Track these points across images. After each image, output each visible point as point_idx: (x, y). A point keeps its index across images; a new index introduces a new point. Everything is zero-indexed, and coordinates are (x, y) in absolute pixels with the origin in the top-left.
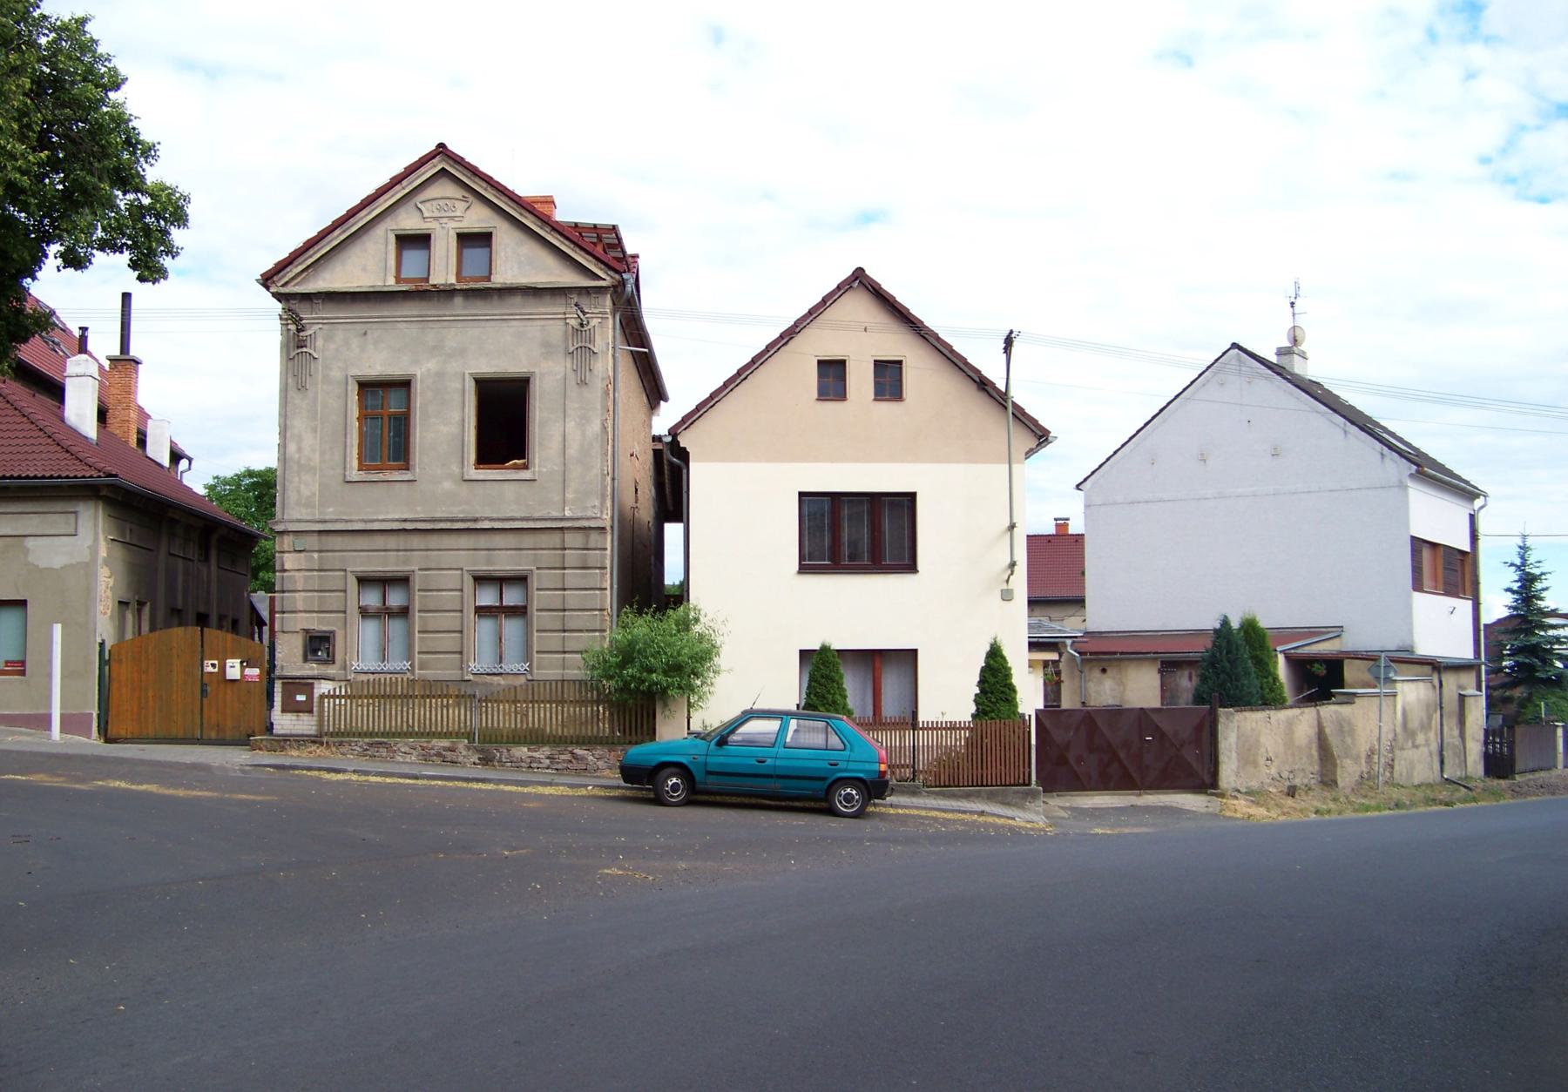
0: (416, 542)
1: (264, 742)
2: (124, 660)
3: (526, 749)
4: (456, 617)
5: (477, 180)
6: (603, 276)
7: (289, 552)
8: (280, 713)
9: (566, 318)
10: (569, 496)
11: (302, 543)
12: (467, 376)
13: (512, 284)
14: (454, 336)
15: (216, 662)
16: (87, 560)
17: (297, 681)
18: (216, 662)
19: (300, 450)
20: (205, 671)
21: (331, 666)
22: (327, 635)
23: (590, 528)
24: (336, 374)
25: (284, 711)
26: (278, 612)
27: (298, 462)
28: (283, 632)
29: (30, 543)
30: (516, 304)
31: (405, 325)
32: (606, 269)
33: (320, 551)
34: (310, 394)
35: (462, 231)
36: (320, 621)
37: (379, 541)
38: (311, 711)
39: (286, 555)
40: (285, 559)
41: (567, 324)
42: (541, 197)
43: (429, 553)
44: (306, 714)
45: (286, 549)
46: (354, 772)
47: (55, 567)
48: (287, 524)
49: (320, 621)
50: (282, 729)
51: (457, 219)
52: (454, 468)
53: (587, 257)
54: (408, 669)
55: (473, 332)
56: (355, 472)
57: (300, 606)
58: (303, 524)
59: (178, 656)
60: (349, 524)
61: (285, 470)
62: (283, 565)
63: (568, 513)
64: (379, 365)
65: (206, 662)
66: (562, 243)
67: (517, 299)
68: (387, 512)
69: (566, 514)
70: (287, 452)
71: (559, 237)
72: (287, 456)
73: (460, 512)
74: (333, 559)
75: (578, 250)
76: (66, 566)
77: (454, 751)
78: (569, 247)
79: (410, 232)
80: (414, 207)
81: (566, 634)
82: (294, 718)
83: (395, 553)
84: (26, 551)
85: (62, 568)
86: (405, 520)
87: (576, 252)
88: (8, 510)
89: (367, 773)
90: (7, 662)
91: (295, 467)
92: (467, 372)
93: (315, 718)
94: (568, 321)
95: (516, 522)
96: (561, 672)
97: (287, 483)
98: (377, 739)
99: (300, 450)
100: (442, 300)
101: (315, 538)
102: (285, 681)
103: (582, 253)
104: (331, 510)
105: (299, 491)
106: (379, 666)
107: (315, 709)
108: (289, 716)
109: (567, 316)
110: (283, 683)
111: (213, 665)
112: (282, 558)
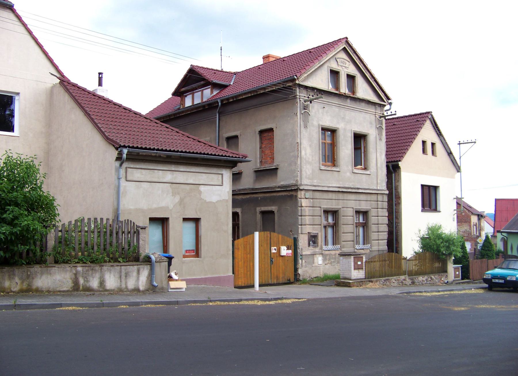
0: (340, 196)
1: (355, 283)
2: (240, 248)
3: (421, 277)
4: (351, 227)
5: (355, 55)
6: (386, 101)
7: (303, 198)
8: (353, 270)
9: (375, 115)
10: (379, 181)
11: (308, 195)
12: (352, 131)
13: (365, 98)
14: (349, 114)
15: (276, 248)
16: (227, 199)
17: (358, 256)
18: (276, 248)
19: (306, 154)
20: (272, 252)
21: (317, 248)
22: (316, 235)
23: (379, 193)
24: (315, 123)
25: (355, 269)
26: (299, 225)
27: (305, 160)
28: (302, 234)
29: (202, 188)
30: (363, 106)
31: (335, 107)
32: (387, 99)
33: (312, 199)
34: (308, 130)
35: (349, 74)
36: (313, 229)
37: (330, 195)
38: (362, 269)
39: (302, 200)
40: (302, 201)
41: (376, 116)
42: (278, 56)
43: (344, 201)
44: (361, 270)
45: (303, 197)
46: (425, 292)
47: (214, 202)
48: (304, 186)
49: (313, 229)
50: (354, 277)
51: (347, 68)
52: (350, 167)
53: (382, 93)
54: (339, 248)
55: (353, 114)
56: (362, 166)
57: (307, 223)
58: (309, 186)
59: (262, 246)
60: (323, 188)
61: (301, 162)
62: (301, 204)
63: (378, 188)
64: (328, 123)
65: (272, 248)
66: (376, 86)
67: (363, 104)
68: (332, 184)
69: (378, 188)
70: (302, 154)
71: (375, 83)
72: (302, 156)
73: (352, 185)
74: (317, 203)
75: (380, 90)
76: (218, 201)
77: (405, 280)
78: (378, 88)
79: (334, 70)
80: (335, 59)
81: (379, 233)
82: (358, 272)
83: (342, 201)
84: (200, 193)
85: (216, 202)
86: (339, 187)
87: (379, 90)
88: (191, 170)
89: (452, 290)
90: (186, 251)
91: (305, 161)
92: (353, 130)
93: (364, 271)
94: (376, 116)
95: (331, 188)
96: (378, 247)
97: (302, 168)
98: (387, 278)
99: (306, 154)
100: (352, 101)
101: (311, 193)
102: (355, 256)
103: (381, 91)
104: (315, 181)
105: (306, 172)
106: (332, 247)
107: (364, 267)
108: (356, 271)
109: (376, 114)
110: (354, 257)
111: (275, 249)
112: (301, 201)
